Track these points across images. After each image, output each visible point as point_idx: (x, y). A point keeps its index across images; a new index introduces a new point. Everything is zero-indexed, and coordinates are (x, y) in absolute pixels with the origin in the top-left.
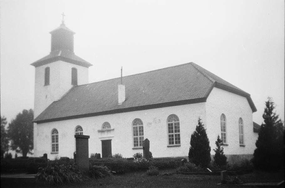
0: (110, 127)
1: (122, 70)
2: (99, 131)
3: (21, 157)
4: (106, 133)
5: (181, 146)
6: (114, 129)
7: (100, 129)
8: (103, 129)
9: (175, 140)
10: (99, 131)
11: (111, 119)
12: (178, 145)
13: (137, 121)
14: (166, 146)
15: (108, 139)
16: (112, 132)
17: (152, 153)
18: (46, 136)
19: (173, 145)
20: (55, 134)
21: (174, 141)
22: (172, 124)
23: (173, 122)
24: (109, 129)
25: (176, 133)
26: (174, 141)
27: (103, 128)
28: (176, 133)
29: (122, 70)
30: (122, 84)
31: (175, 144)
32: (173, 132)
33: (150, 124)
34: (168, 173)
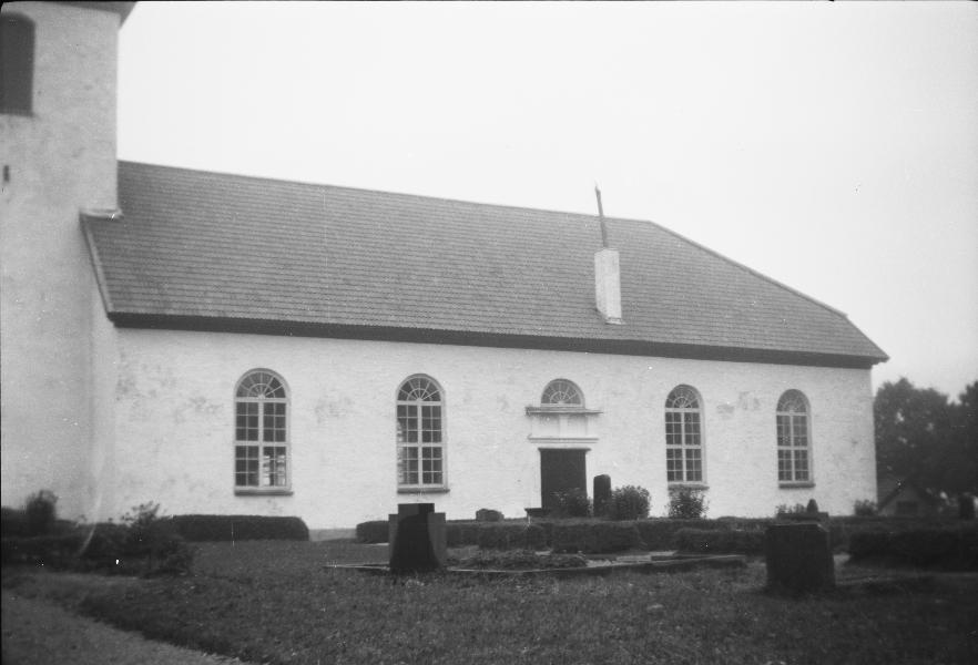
0: (576, 400)
1: (598, 193)
2: (531, 412)
3: (945, 491)
4: (564, 422)
5: (296, 494)
6: (595, 414)
7: (537, 403)
8: (546, 405)
9: (424, 469)
10: (531, 412)
11: (586, 372)
12: (803, 482)
13: (682, 396)
14: (395, 489)
15: (569, 446)
16: (592, 423)
17: (298, 515)
18: (198, 403)
19: (789, 482)
20: (791, 413)
21: (793, 470)
22: (677, 416)
23: (682, 410)
24: (573, 407)
25: (427, 445)
26: (793, 470)
27: (545, 399)
28: (427, 445)
29: (598, 193)
30: (605, 245)
31: (794, 481)
32: (796, 452)
33: (730, 409)
34: (556, 589)
